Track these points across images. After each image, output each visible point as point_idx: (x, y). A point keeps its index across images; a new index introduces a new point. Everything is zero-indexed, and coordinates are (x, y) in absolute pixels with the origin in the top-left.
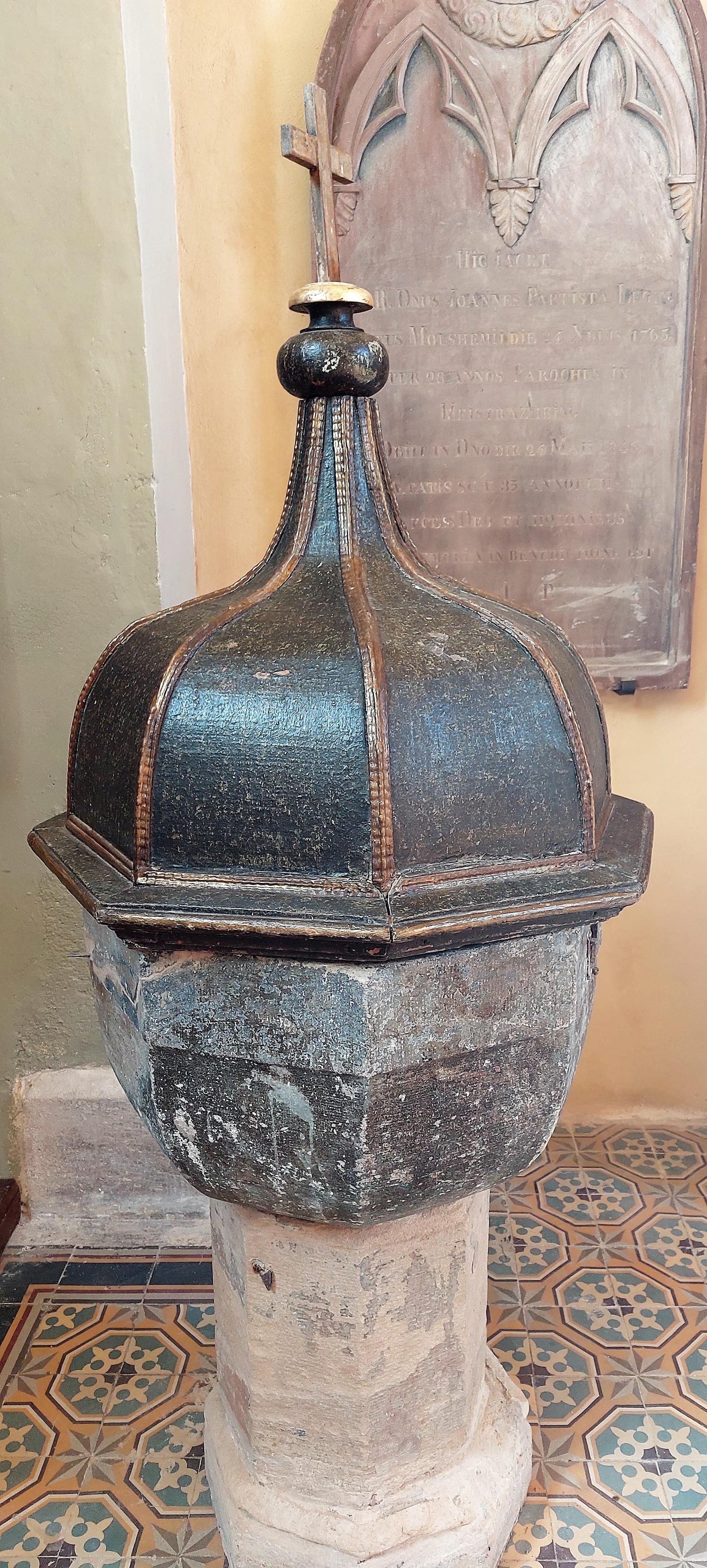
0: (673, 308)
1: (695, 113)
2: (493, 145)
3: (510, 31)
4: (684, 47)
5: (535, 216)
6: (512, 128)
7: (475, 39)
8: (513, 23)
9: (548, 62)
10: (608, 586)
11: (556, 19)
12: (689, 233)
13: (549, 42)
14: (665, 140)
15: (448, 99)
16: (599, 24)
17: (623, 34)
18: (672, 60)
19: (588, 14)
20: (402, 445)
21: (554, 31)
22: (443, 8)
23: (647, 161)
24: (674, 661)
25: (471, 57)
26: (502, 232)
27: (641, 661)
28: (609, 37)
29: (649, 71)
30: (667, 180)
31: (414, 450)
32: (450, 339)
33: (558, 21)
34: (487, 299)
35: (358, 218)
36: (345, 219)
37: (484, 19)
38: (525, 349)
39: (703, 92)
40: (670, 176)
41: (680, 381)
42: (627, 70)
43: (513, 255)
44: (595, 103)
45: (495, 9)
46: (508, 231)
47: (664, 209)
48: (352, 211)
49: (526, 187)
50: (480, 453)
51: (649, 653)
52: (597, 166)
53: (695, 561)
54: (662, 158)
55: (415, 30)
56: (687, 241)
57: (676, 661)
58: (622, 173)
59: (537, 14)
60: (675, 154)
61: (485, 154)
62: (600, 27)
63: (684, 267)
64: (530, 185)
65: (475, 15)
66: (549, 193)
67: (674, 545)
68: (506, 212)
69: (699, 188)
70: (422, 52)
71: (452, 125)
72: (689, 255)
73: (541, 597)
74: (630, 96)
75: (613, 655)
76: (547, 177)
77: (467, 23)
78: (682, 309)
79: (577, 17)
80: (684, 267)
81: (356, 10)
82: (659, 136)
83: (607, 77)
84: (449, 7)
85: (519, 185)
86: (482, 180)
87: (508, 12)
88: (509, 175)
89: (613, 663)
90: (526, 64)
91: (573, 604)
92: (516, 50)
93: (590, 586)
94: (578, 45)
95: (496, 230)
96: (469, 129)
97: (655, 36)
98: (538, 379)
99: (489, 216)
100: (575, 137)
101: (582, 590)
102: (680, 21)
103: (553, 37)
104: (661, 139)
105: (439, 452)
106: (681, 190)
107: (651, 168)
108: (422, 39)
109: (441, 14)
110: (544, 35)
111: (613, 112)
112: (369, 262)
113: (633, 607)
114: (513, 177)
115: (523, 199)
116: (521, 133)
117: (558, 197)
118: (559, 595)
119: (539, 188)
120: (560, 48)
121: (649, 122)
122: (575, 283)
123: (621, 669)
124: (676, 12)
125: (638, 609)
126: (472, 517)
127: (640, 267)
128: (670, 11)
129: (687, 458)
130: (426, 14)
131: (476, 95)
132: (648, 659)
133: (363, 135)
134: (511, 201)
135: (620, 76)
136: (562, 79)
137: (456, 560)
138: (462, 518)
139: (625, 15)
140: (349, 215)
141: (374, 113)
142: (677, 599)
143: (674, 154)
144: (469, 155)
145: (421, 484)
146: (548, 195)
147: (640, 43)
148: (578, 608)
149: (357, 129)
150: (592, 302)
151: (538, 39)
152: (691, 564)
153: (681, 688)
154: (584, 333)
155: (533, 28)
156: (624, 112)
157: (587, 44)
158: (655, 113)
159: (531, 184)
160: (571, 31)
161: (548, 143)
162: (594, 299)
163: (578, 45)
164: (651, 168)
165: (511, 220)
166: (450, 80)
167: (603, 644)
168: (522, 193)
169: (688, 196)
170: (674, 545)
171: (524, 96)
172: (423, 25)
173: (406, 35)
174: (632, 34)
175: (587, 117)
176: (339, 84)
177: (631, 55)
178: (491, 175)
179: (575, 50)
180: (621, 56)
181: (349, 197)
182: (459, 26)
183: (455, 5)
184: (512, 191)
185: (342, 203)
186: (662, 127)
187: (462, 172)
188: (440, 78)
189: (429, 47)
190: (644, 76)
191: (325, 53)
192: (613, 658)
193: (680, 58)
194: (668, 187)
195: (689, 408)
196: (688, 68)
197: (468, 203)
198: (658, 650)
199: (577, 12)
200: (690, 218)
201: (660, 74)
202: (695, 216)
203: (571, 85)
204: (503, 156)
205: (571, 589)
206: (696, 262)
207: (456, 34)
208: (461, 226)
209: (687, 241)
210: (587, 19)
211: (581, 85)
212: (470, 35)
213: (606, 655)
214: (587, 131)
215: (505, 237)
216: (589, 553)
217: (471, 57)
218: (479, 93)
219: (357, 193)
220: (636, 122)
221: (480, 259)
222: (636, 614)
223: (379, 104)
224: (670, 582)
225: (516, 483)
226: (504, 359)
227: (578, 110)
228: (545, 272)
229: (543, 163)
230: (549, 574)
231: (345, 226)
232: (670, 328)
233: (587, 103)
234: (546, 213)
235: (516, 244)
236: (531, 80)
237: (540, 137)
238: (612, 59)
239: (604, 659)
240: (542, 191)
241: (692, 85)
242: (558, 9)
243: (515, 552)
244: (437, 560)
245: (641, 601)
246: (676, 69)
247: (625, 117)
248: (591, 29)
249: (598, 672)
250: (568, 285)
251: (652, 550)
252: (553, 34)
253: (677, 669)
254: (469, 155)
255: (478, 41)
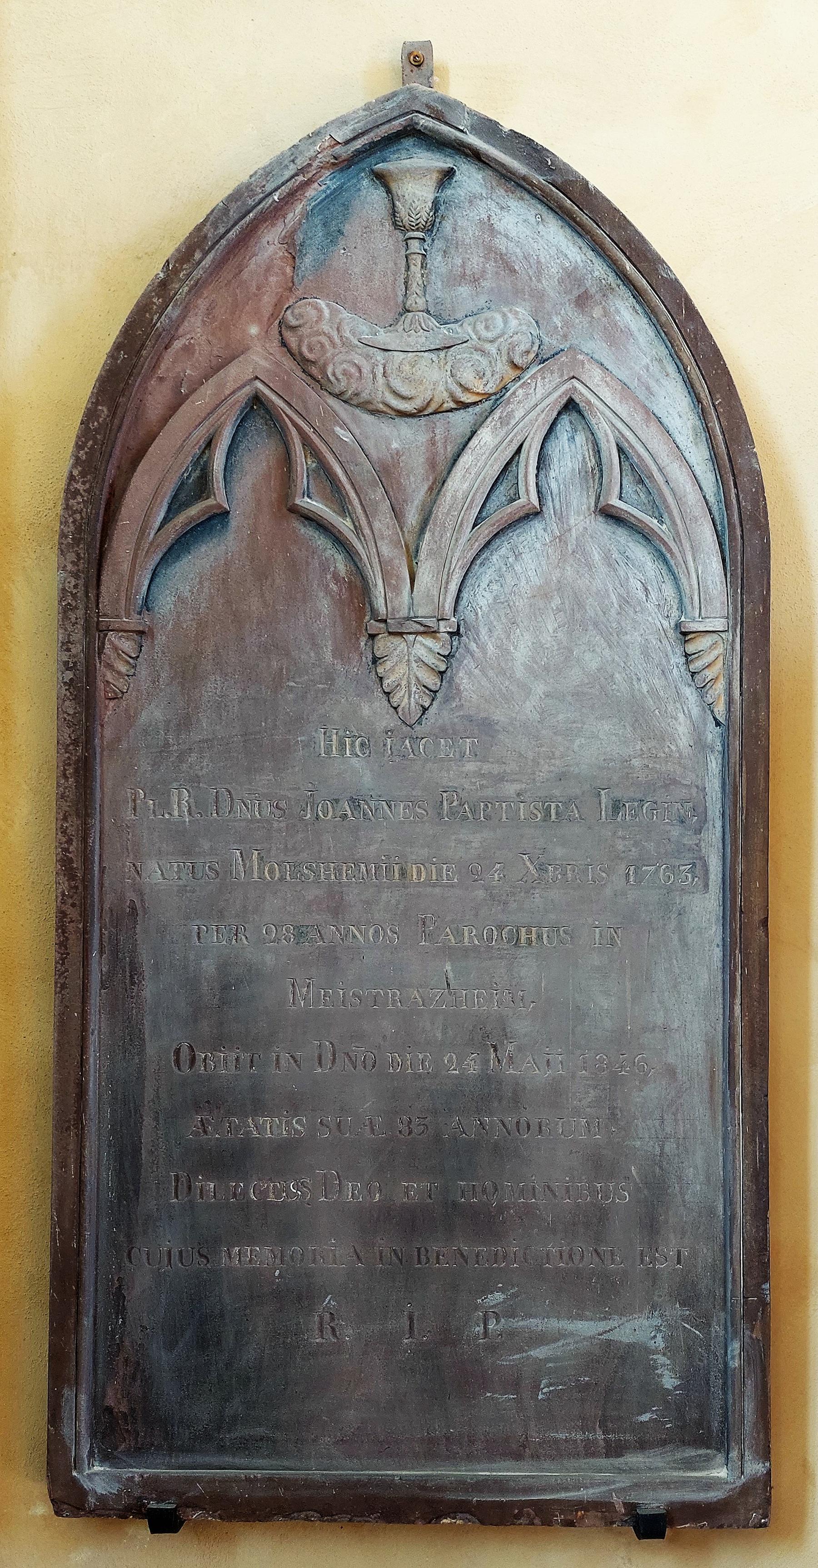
0: (699, 831)
1: (722, 523)
2: (377, 568)
3: (404, 390)
4: (698, 423)
5: (452, 678)
6: (411, 539)
7: (345, 402)
8: (407, 380)
9: (470, 439)
10: (605, 1318)
11: (481, 375)
12: (720, 709)
13: (470, 409)
14: (672, 562)
15: (300, 492)
16: (554, 384)
17: (593, 400)
18: (678, 441)
19: (534, 370)
20: (215, 1049)
21: (478, 394)
22: (292, 354)
23: (641, 595)
24: (738, 1473)
25: (337, 429)
26: (395, 701)
27: (675, 1469)
28: (570, 406)
29: (639, 456)
30: (678, 625)
31: (237, 1059)
32: (306, 871)
33: (485, 379)
34: (369, 807)
35: (143, 671)
36: (119, 673)
37: (360, 371)
38: (437, 890)
39: (733, 491)
40: (683, 619)
41: (718, 953)
42: (604, 454)
43: (415, 739)
44: (550, 504)
45: (379, 358)
46: (406, 700)
47: (675, 671)
48: (131, 661)
49: (433, 632)
50: (360, 1067)
51: (690, 1452)
52: (556, 602)
53: (766, 1278)
54: (669, 590)
55: (243, 386)
56: (718, 724)
57: (742, 1473)
58: (600, 613)
59: (448, 368)
60: (691, 586)
61: (364, 579)
62: (555, 389)
63: (714, 764)
64: (442, 629)
65: (345, 366)
66: (475, 640)
67: (726, 1246)
68: (402, 669)
69: (733, 641)
70: (258, 419)
71: (306, 531)
72: (723, 745)
73: (477, 1337)
74: (609, 493)
75: (619, 1455)
76: (470, 617)
77: (332, 378)
78: (714, 834)
79: (518, 372)
80: (714, 765)
81: (144, 352)
82: (661, 557)
83: (570, 464)
84: (301, 354)
85: (422, 629)
86: (360, 619)
87: (401, 363)
88: (404, 613)
89: (620, 1471)
90: (433, 442)
91: (540, 1353)
92: (416, 420)
93: (571, 1318)
94: (518, 414)
95: (385, 697)
96: (337, 538)
97: (646, 403)
98: (462, 941)
99: (373, 676)
100: (518, 556)
101: (554, 1324)
102: (689, 384)
103: (475, 404)
104: (666, 562)
105: (282, 1062)
106: (703, 643)
107: (650, 606)
108: (257, 399)
109: (288, 363)
110: (462, 399)
111: (582, 518)
112: (161, 743)
113: (655, 1360)
114: (412, 614)
115: (430, 650)
116: (424, 547)
117: (491, 648)
118: (512, 1334)
119: (457, 633)
120: (490, 419)
121: (645, 535)
122: (524, 786)
123: (636, 1486)
124: (682, 370)
125: (663, 1365)
126: (345, 1182)
127: (636, 762)
128: (671, 369)
129: (739, 1089)
130: (264, 363)
131: (348, 487)
132: (689, 1464)
133: (151, 544)
134: (409, 654)
135: (591, 463)
136: (492, 466)
137: (314, 1261)
138: (325, 1184)
139: (597, 373)
140: (127, 667)
141: (174, 508)
142: (737, 1352)
143: (689, 584)
144: (336, 577)
145: (250, 1120)
146: (473, 646)
147: (624, 416)
148: (547, 1360)
149: (143, 532)
150: (553, 817)
151: (452, 405)
152: (759, 1285)
153: (755, 1527)
154: (542, 868)
155: (443, 389)
156: (600, 519)
157: (534, 414)
158: (654, 523)
159: (443, 627)
160: (508, 394)
161: (472, 563)
162: (557, 814)
163: (518, 414)
164: (650, 606)
165: (409, 683)
166: (302, 462)
167: (599, 1432)
168: (429, 642)
169: (716, 653)
170: (726, 1246)
171: (431, 489)
172: (257, 378)
173: (227, 392)
174: (608, 401)
175: (537, 526)
176: (114, 461)
177: (609, 432)
178: (373, 611)
179: (513, 422)
180: (593, 434)
181: (128, 639)
182: (321, 383)
183: (311, 350)
184: (411, 637)
185: (116, 648)
186: (665, 544)
187: (324, 605)
188: (287, 460)
189: (267, 411)
190: (631, 465)
191: (90, 414)
192: (621, 1460)
193: (691, 439)
194: (680, 636)
195: (738, 1001)
196: (706, 454)
197: (337, 653)
198: (708, 1448)
199: (515, 366)
200: (720, 686)
201: (660, 461)
202: (730, 684)
203: (510, 477)
204: (394, 582)
205: (535, 1324)
206: (735, 758)
207: (312, 395)
208: (323, 689)
209: (718, 724)
210: (533, 377)
211: (526, 476)
212: (338, 396)
213: (607, 1456)
214: (538, 545)
215: (400, 709)
216: (566, 1256)
217: (337, 429)
218: (352, 484)
219: (141, 633)
220: (622, 535)
221: (357, 743)
222: (661, 1375)
223: (182, 497)
224: (722, 1314)
225: (426, 1121)
226: (401, 907)
227: (522, 514)
228: (471, 767)
229: (465, 595)
230: (492, 1293)
231: (119, 685)
232: (694, 864)
233: (536, 503)
234: (470, 674)
235: (419, 721)
236: (442, 467)
237: (457, 554)
238: (577, 438)
239: (603, 1462)
240: (464, 638)
241: (714, 480)
242: (484, 362)
243: (427, 1251)
244: (278, 1261)
245: (670, 1350)
246: (686, 454)
247: (601, 526)
248: (540, 392)
249: (591, 1491)
250: (511, 789)
251: (685, 1253)
252: (478, 398)
253: (745, 1490)
254: (336, 577)
255: (351, 405)
